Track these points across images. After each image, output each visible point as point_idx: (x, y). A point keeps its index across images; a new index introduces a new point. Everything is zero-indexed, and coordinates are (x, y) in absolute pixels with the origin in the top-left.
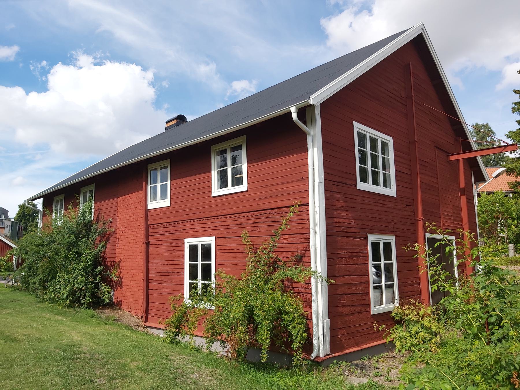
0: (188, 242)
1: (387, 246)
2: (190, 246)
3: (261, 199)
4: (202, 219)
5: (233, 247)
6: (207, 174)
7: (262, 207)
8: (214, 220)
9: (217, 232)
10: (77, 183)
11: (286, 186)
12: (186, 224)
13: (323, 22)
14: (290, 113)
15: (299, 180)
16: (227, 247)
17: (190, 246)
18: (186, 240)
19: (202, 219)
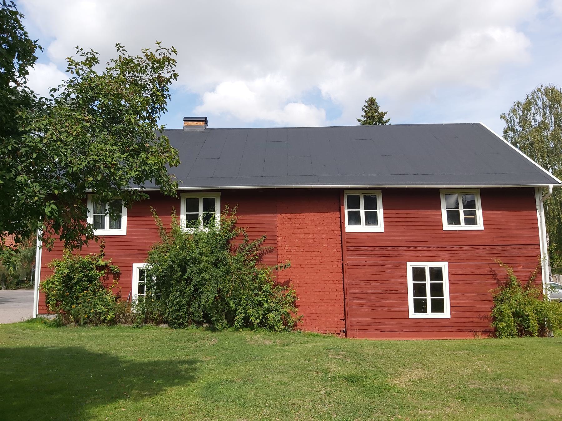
0: (410, 266)
1: (436, 274)
2: (413, 268)
3: (496, 237)
4: (429, 246)
5: (467, 271)
6: (438, 211)
7: (499, 243)
8: (446, 249)
9: (449, 258)
10: (427, 188)
11: (520, 231)
12: (404, 249)
13: (170, 120)
14: (548, 188)
15: (530, 229)
16: (461, 271)
17: (413, 268)
18: (446, 263)
19: (429, 246)
